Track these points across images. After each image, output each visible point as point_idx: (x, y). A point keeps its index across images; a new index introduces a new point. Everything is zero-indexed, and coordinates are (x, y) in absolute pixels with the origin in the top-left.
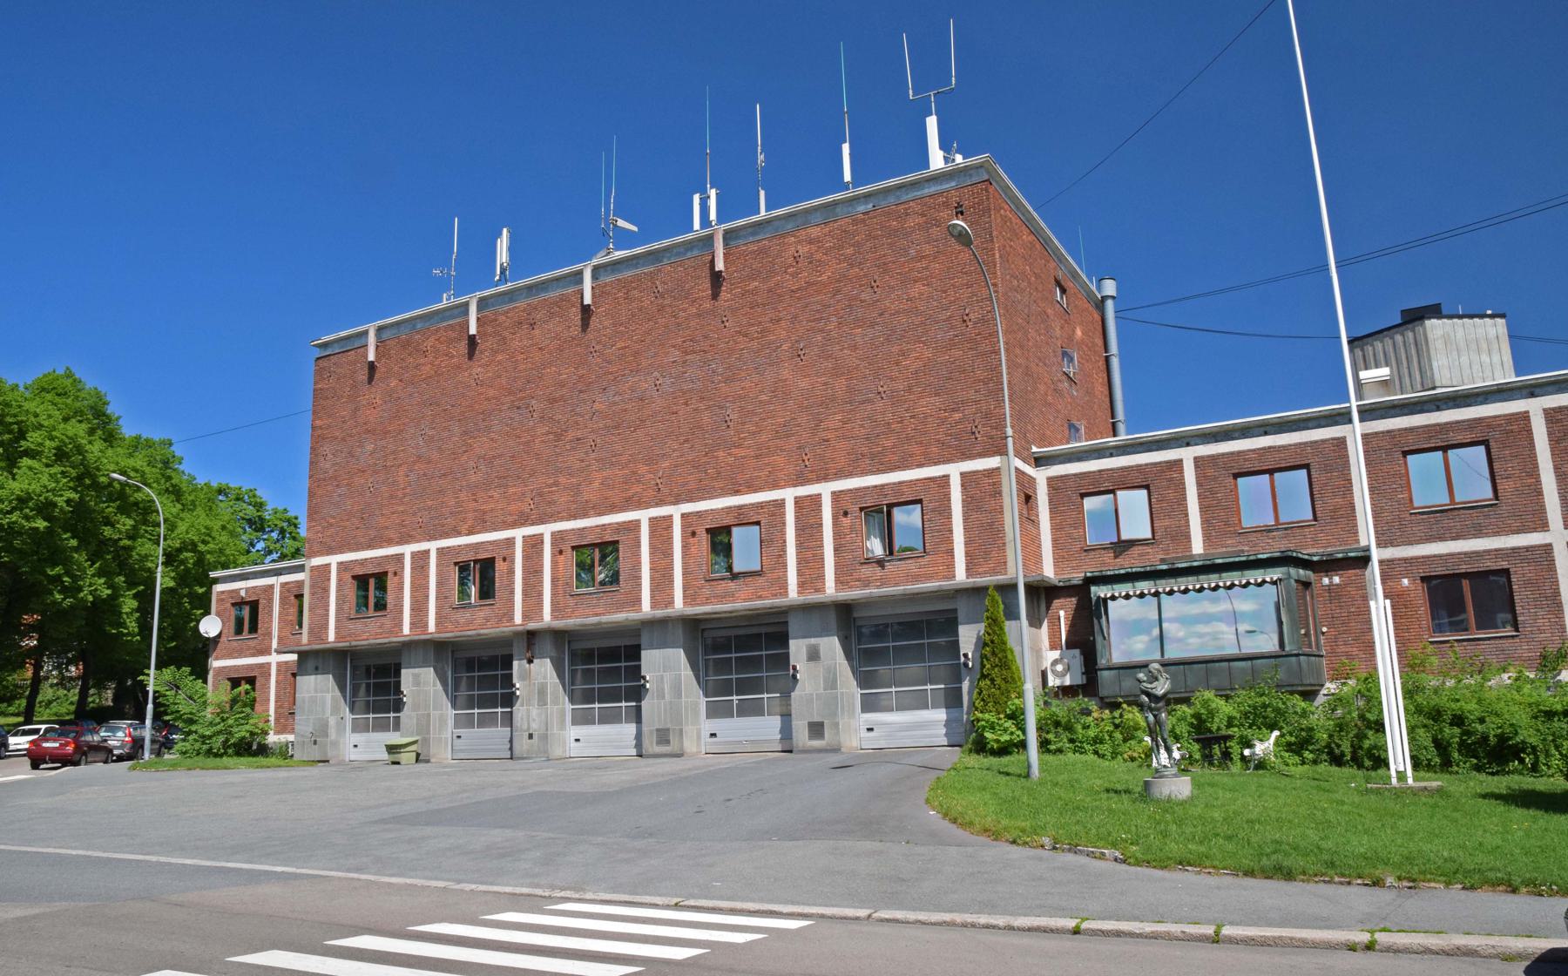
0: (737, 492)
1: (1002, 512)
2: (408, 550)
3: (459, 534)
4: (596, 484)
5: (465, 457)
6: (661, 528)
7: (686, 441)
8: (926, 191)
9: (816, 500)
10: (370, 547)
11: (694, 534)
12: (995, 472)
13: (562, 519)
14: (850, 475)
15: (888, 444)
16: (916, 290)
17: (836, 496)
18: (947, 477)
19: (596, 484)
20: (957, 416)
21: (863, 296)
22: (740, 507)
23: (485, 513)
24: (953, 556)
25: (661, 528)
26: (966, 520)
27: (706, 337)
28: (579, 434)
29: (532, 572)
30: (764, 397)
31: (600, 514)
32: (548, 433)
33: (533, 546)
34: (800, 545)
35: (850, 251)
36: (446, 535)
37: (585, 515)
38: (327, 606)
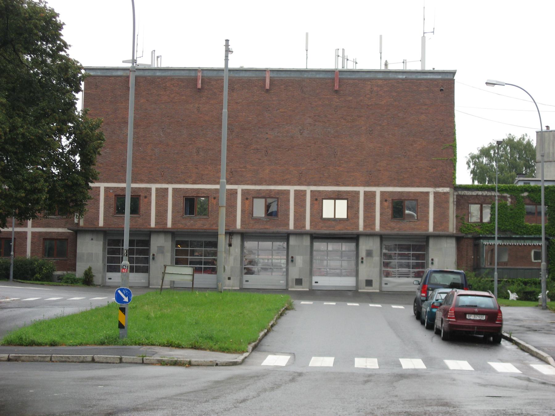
0: (338, 185)
1: (448, 209)
2: (153, 187)
3: (187, 183)
4: (267, 171)
5: (190, 146)
6: (162, 194)
7: (314, 159)
8: (429, 77)
9: (235, 192)
10: (255, 184)
11: (316, 200)
12: (217, 190)
13: (248, 184)
14: (389, 186)
15: (405, 176)
16: (423, 117)
17: (382, 193)
18: (306, 191)
19: (267, 171)
20: (434, 170)
21: (399, 115)
22: (339, 192)
23: (202, 175)
24: (428, 223)
25: (162, 194)
26: (434, 210)
27: (326, 116)
28: (258, 147)
29: (231, 206)
30: (352, 148)
31: (268, 185)
32: (240, 143)
33: (231, 194)
34: (365, 211)
35: (395, 94)
36: (179, 182)
37: (260, 184)
38: (98, 208)
